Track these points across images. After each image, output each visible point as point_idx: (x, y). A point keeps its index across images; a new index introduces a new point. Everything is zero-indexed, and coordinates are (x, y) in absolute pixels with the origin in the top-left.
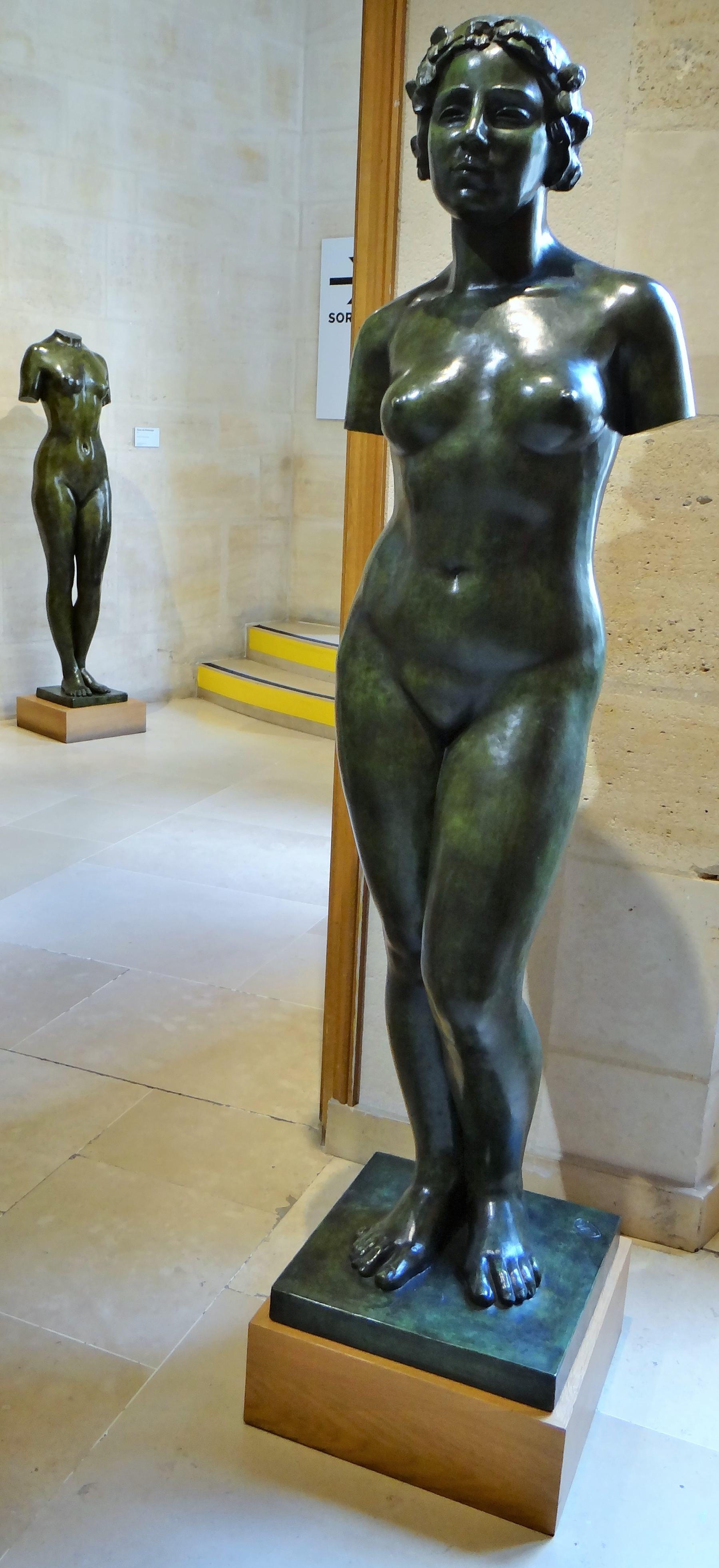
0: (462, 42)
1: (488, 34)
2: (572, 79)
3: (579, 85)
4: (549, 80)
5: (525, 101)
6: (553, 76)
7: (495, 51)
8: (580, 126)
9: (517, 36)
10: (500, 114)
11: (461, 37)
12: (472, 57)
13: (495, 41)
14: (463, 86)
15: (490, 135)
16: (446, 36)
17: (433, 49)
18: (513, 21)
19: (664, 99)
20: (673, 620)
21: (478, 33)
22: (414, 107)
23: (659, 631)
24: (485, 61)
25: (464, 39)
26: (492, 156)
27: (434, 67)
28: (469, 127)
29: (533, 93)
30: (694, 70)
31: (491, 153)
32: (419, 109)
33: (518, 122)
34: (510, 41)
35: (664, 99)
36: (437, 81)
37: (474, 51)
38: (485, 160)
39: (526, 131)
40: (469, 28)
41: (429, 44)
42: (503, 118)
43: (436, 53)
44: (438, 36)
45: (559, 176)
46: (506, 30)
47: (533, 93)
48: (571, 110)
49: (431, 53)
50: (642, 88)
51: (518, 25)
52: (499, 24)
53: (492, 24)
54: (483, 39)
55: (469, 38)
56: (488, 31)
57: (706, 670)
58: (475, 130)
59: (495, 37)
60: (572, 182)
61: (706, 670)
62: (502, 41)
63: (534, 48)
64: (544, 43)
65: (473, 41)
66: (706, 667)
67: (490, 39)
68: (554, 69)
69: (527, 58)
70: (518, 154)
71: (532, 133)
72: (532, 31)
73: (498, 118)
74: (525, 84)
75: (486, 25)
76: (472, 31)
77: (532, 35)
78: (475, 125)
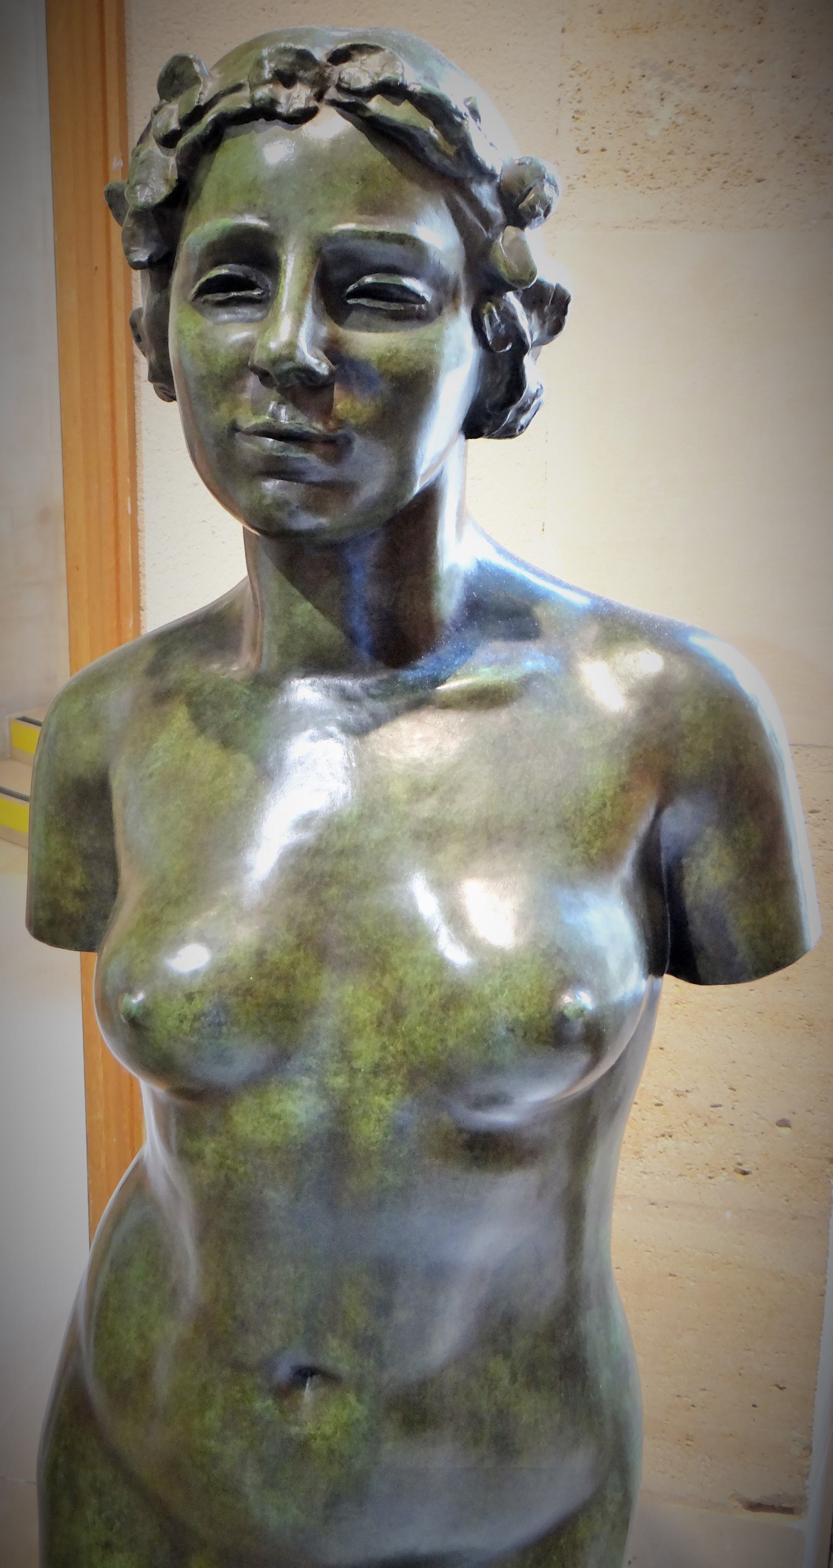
0: (241, 101)
1: (312, 83)
2: (531, 196)
3: (547, 211)
4: (474, 202)
5: (415, 255)
6: (485, 193)
7: (330, 126)
8: (552, 306)
9: (392, 90)
10: (356, 294)
11: (238, 88)
12: (269, 140)
13: (334, 103)
14: (251, 220)
15: (333, 350)
16: (196, 80)
17: (164, 114)
18: (375, 49)
19: (626, 171)
20: (681, 1088)
21: (286, 79)
22: (128, 252)
23: (658, 1105)
24: (309, 158)
25: (246, 93)
26: (346, 404)
27: (172, 161)
28: (277, 335)
29: (437, 234)
30: (680, 120)
31: (337, 393)
32: (142, 256)
33: (404, 310)
34: (376, 105)
35: (626, 171)
36: (181, 197)
37: (277, 127)
38: (327, 412)
39: (425, 332)
40: (259, 64)
41: (155, 98)
42: (363, 301)
43: (174, 125)
44: (175, 78)
45: (495, 411)
46: (360, 73)
47: (437, 234)
48: (533, 274)
49: (159, 124)
50: (582, 149)
51: (390, 61)
52: (340, 57)
53: (320, 55)
54: (298, 97)
55: (263, 92)
56: (309, 74)
57: (745, 1173)
58: (292, 345)
59: (332, 93)
60: (523, 421)
61: (745, 1173)
62: (353, 106)
63: (436, 123)
64: (463, 110)
65: (274, 102)
66: (745, 1168)
67: (319, 97)
68: (483, 173)
69: (419, 145)
70: (407, 393)
71: (438, 340)
72: (430, 77)
73: (351, 302)
74: (412, 215)
75: (304, 57)
76: (267, 75)
77: (430, 87)
78: (292, 328)
